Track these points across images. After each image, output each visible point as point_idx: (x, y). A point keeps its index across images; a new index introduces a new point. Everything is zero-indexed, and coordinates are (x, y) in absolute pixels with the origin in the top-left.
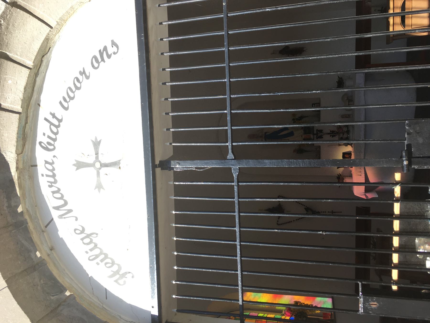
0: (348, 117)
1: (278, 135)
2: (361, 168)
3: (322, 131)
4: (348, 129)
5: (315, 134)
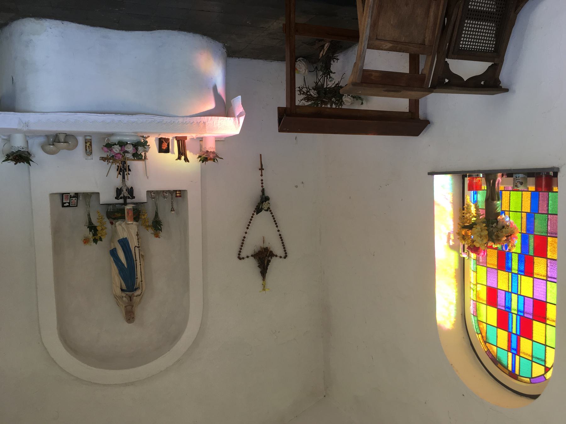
0: (91, 143)
1: (126, 266)
2: (192, 123)
4: (115, 144)
5: (125, 201)
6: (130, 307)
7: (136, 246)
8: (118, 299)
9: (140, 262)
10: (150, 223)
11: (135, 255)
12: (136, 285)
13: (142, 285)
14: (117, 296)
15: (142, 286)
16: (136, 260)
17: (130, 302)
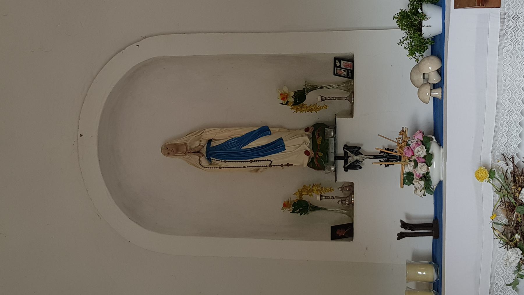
3: (360, 151)
6: (185, 150)
7: (271, 162)
8: (199, 134)
9: (248, 167)
10: (306, 198)
11: (259, 161)
12: (215, 159)
13: (215, 168)
14: (202, 133)
15: (213, 168)
16: (251, 161)
17: (192, 151)
